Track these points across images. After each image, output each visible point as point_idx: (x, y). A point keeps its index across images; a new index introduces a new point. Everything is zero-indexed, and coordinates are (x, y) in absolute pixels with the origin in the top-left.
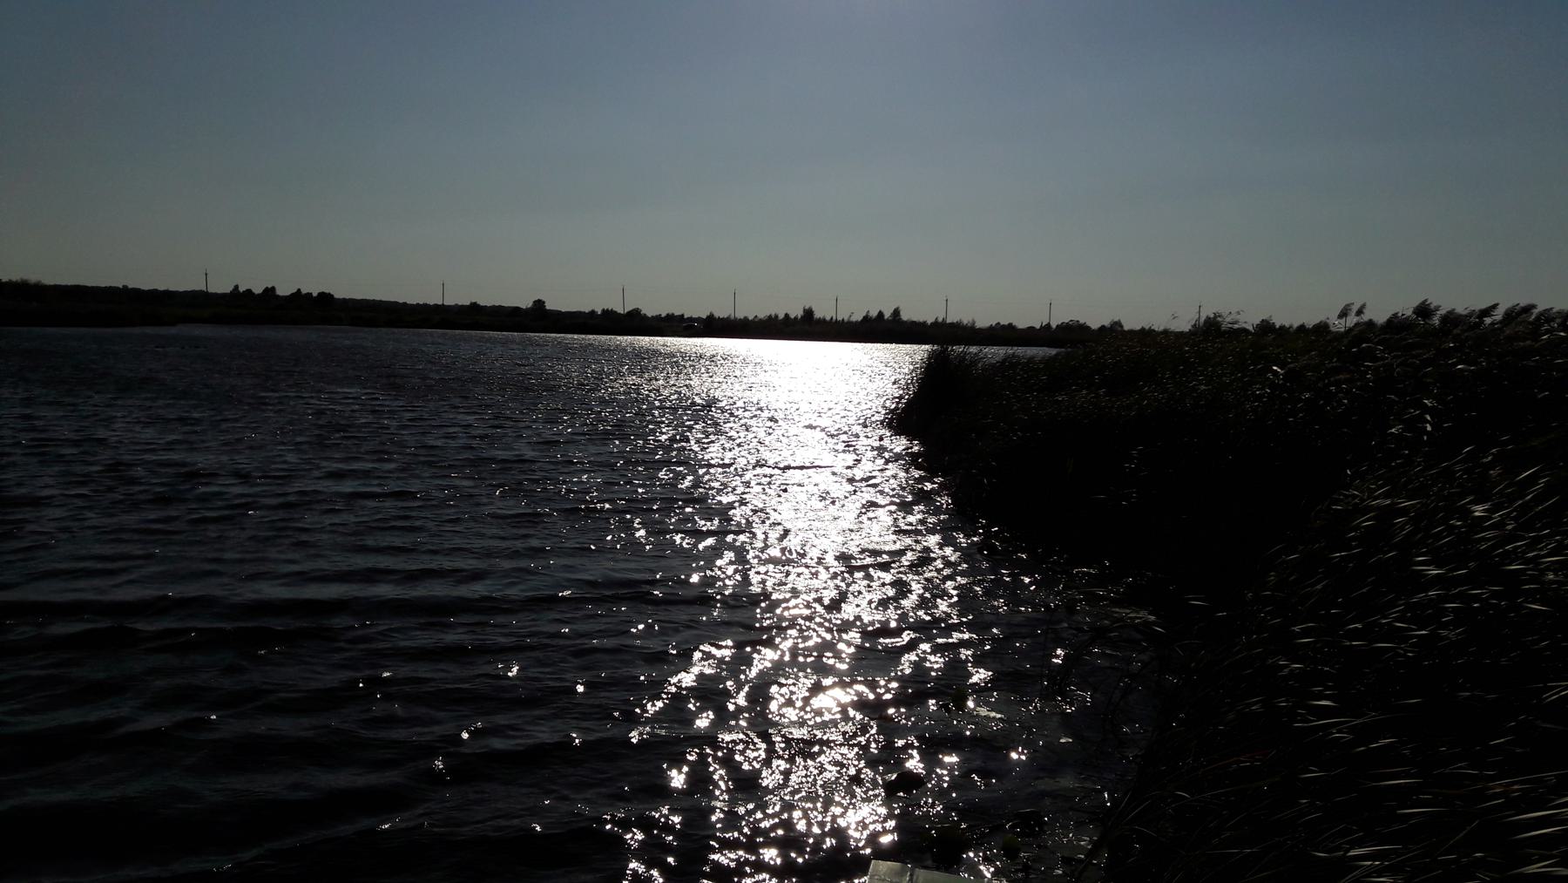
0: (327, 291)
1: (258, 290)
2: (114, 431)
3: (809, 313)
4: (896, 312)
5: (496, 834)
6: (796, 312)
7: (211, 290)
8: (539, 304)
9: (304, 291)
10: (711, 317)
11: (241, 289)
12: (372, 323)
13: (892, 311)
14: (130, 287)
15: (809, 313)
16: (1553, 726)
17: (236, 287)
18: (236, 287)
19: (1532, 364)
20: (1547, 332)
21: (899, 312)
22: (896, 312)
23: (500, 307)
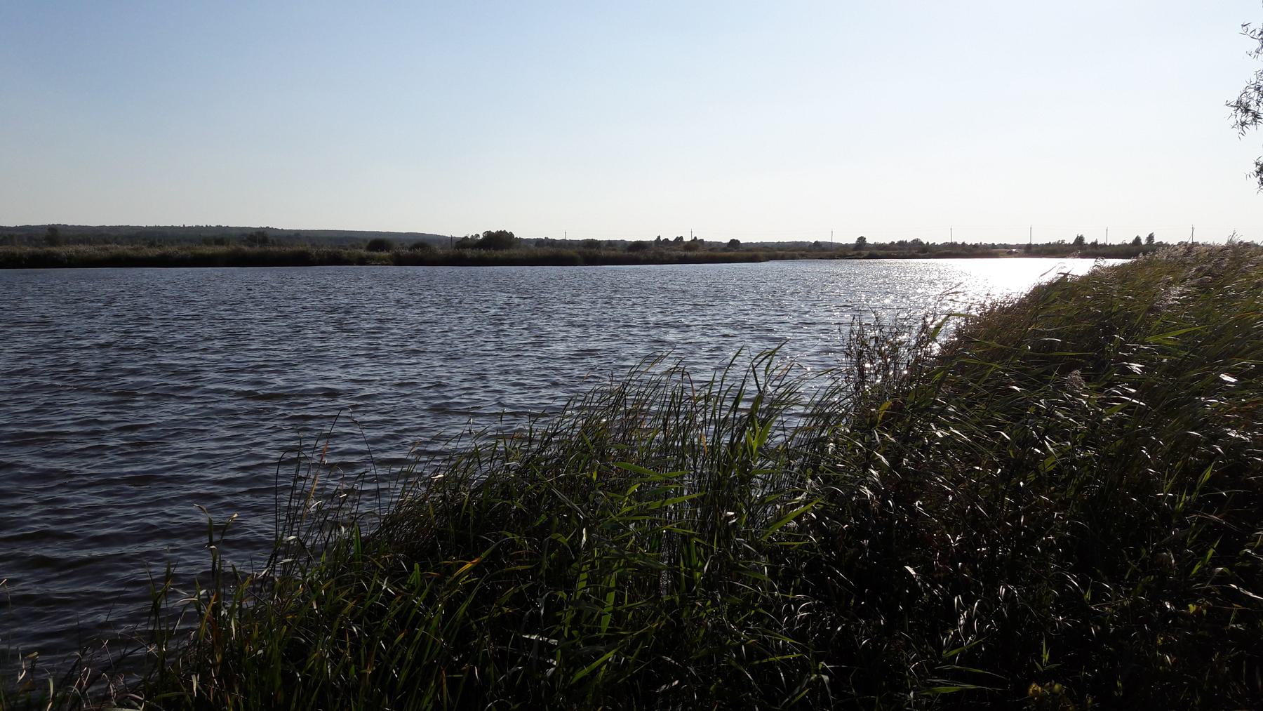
0: (736, 239)
1: (672, 239)
2: (239, 341)
3: (1080, 240)
4: (1151, 238)
5: (68, 610)
6: (1070, 240)
7: (833, 241)
8: (862, 239)
9: (698, 238)
10: (734, 243)
11: (983, 244)
12: (754, 259)
13: (1148, 236)
14: (550, 238)
15: (1080, 240)
16: (982, 671)
17: (659, 237)
18: (659, 237)
19: (123, 625)
20: (1247, 453)
21: (1153, 237)
22: (1151, 238)
23: (104, 226)
